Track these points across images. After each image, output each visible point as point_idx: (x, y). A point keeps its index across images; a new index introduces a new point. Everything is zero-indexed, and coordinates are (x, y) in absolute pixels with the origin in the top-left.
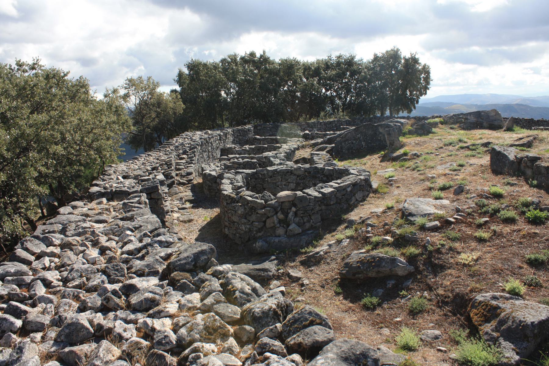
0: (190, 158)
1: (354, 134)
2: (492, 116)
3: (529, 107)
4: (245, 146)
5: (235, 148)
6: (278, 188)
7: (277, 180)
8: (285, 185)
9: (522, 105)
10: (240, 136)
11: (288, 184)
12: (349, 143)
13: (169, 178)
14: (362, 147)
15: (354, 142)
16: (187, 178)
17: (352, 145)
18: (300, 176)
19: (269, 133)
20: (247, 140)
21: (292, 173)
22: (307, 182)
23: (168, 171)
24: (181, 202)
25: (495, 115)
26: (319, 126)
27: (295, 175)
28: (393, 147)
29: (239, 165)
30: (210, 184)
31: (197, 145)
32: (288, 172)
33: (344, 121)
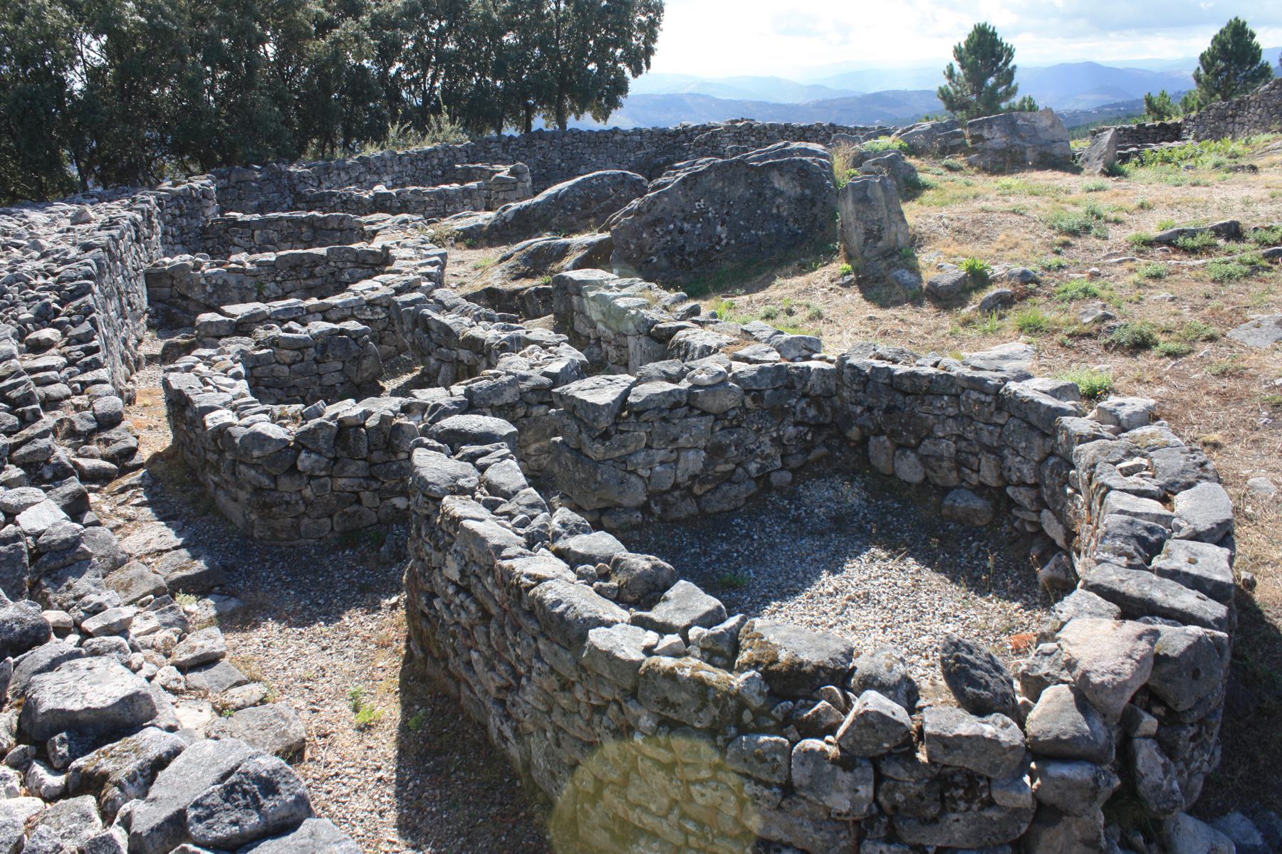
0: (79, 340)
1: (683, 200)
2: (1046, 130)
3: (715, 99)
4: (233, 258)
5: (197, 266)
6: (633, 479)
7: (631, 448)
8: (662, 463)
9: (699, 95)
10: (181, 216)
11: (674, 455)
12: (670, 232)
13: (48, 475)
14: (718, 243)
15: (687, 226)
16: (107, 442)
17: (681, 240)
18: (725, 413)
19: (257, 198)
20: (204, 229)
21: (691, 408)
22: (752, 437)
23: (28, 440)
24: (170, 617)
25: (1052, 126)
26: (396, 169)
27: (704, 413)
28: (880, 244)
29: (299, 349)
30: (266, 482)
31: (88, 276)
32: (677, 405)
33: (460, 150)
